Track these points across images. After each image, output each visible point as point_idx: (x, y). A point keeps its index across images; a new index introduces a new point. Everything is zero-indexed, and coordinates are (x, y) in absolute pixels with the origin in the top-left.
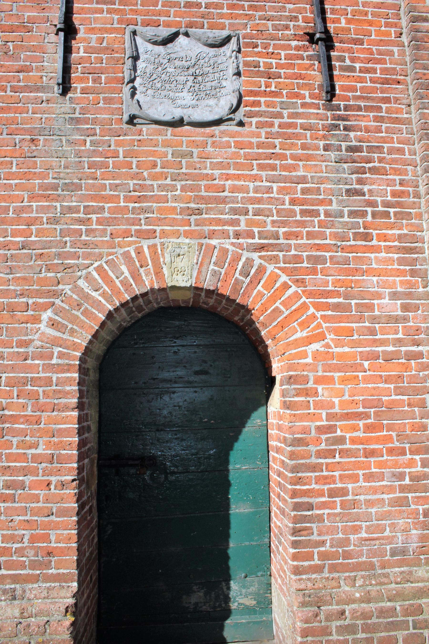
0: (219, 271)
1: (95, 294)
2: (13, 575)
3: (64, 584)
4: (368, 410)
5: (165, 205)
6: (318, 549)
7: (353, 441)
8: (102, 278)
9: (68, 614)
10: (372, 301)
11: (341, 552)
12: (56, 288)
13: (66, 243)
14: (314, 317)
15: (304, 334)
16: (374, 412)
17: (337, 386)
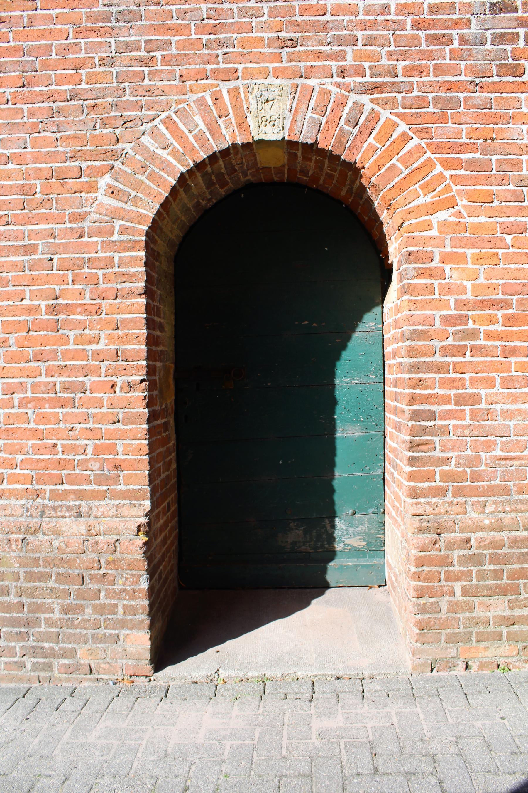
0: (318, 119)
1: (164, 154)
2: (77, 490)
3: (135, 502)
4: (509, 297)
5: (249, 35)
6: (440, 468)
7: (489, 336)
8: (170, 132)
9: (140, 533)
10: (519, 157)
11: (469, 472)
12: (115, 147)
13: (124, 90)
14: (441, 177)
15: (429, 199)
16: (517, 300)
17: (470, 266)
